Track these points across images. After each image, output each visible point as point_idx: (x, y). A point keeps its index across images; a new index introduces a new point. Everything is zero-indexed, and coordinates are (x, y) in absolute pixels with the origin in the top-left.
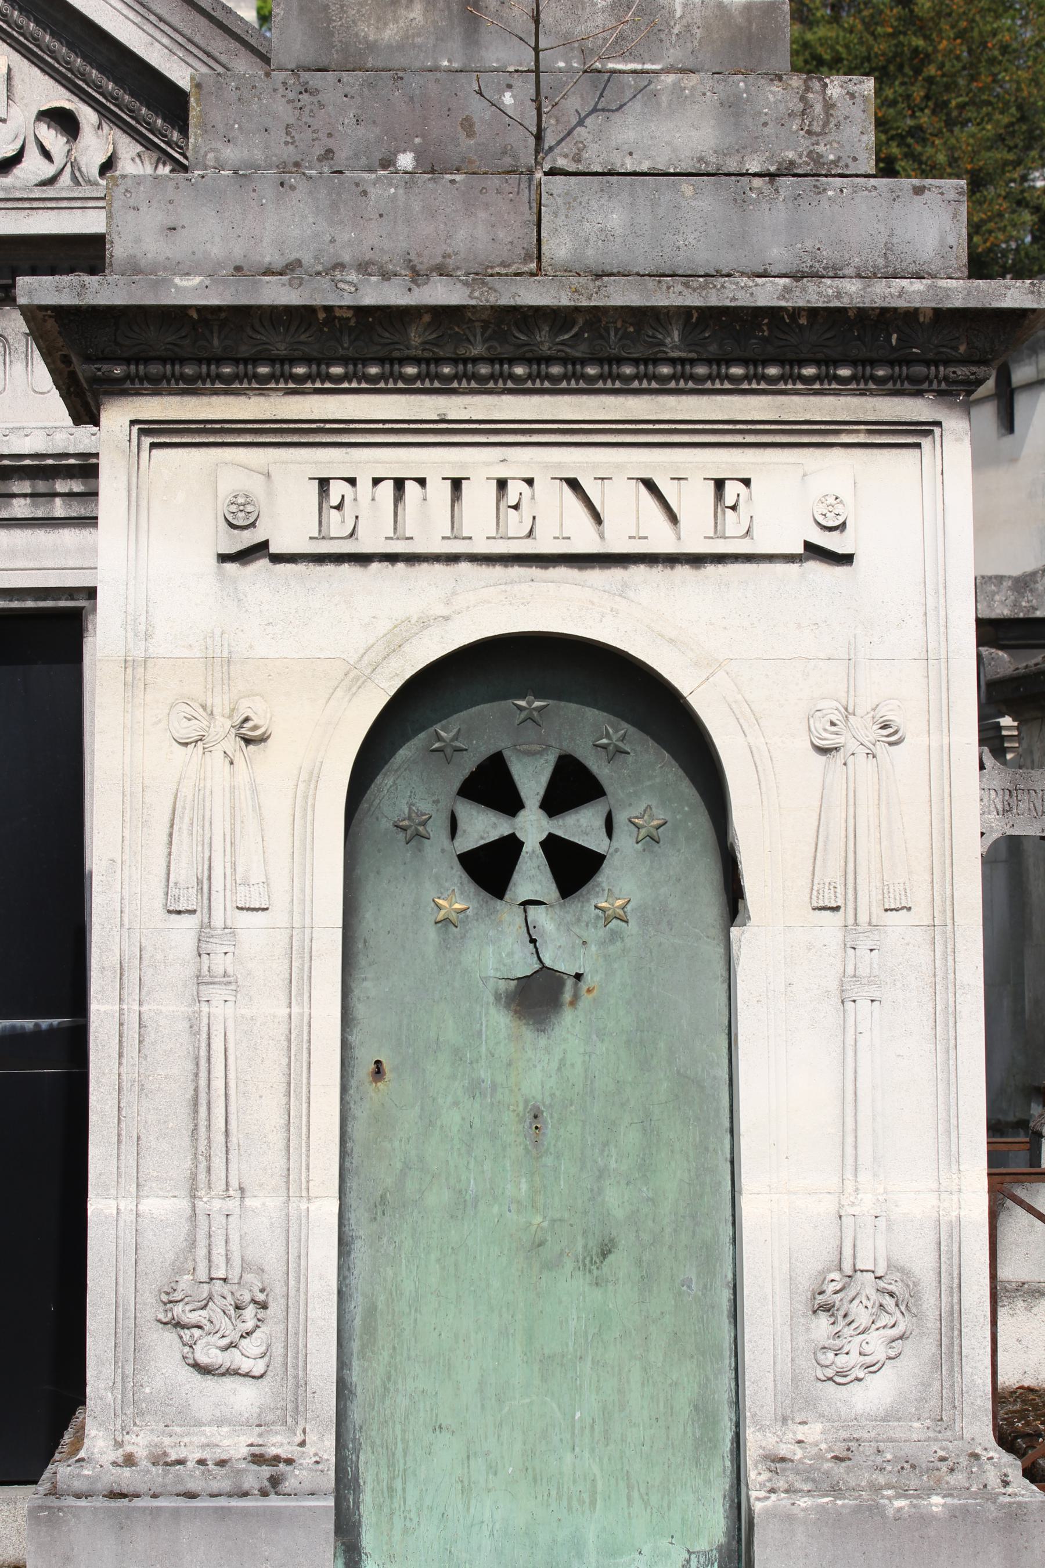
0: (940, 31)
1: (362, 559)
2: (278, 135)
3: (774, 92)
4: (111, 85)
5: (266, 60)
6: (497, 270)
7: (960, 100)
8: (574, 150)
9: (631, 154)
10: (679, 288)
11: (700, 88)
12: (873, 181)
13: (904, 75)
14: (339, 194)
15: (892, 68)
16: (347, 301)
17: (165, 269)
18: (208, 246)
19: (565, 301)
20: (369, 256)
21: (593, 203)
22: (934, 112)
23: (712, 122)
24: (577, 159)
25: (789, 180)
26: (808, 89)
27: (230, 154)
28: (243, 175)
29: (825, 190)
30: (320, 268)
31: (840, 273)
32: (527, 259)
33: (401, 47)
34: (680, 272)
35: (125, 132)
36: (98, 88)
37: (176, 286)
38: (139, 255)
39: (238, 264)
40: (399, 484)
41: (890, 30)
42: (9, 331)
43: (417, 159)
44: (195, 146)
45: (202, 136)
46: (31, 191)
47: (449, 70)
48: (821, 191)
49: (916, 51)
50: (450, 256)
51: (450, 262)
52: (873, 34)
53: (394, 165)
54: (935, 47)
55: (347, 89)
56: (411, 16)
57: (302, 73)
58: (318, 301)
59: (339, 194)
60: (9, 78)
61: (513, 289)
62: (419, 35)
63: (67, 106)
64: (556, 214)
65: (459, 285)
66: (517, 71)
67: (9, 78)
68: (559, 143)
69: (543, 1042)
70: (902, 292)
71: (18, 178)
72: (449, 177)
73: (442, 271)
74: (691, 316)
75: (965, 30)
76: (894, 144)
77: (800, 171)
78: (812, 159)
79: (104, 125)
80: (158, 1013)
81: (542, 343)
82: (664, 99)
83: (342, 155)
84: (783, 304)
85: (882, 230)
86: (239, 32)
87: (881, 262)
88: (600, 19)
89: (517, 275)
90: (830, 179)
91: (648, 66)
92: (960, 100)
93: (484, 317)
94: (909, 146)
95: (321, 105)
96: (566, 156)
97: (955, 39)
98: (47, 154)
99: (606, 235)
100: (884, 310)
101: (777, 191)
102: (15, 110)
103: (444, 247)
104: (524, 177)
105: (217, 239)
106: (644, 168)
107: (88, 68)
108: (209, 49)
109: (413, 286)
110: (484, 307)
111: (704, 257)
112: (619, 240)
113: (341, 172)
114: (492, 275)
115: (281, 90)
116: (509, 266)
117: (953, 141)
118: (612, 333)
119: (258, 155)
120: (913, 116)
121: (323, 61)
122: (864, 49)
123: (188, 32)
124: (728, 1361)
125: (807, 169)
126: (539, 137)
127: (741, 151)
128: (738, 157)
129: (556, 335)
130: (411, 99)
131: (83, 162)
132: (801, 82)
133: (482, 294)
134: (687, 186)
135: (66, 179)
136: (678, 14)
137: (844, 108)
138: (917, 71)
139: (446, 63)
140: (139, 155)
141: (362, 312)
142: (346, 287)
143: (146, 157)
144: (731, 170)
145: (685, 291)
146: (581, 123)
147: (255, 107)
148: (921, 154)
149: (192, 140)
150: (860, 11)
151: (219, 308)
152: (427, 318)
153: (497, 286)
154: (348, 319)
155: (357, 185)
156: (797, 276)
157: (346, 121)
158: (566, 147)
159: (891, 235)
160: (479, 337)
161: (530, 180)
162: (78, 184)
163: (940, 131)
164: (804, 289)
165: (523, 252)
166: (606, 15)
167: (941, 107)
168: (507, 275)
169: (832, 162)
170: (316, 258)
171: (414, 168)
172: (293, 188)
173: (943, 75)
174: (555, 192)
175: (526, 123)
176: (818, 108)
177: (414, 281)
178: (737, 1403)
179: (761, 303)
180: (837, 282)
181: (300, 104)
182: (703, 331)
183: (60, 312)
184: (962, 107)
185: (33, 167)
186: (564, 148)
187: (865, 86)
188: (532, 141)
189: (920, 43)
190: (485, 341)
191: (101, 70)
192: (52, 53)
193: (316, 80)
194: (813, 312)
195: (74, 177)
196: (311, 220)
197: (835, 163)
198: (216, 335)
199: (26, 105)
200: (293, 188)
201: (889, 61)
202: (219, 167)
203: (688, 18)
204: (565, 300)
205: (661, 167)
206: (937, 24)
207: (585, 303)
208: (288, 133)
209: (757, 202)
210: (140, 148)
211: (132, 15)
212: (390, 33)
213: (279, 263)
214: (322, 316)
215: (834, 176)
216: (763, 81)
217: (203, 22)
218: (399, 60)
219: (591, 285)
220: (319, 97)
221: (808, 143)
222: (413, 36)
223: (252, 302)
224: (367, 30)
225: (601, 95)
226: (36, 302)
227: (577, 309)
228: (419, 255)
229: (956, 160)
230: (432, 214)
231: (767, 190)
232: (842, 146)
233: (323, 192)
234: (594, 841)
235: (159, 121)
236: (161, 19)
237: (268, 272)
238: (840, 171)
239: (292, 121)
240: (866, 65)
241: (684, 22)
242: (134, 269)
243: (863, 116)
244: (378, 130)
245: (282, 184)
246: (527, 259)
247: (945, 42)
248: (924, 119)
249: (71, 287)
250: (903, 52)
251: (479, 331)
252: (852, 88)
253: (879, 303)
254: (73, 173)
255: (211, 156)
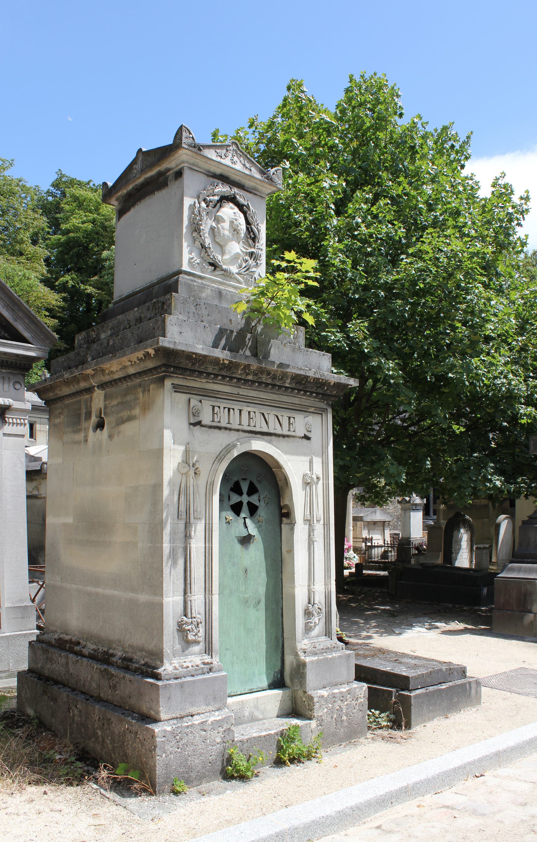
1: (220, 428)
40: (229, 409)
69: (247, 552)
80: (176, 546)
124: (281, 627)
178: (283, 636)
234: (256, 503)
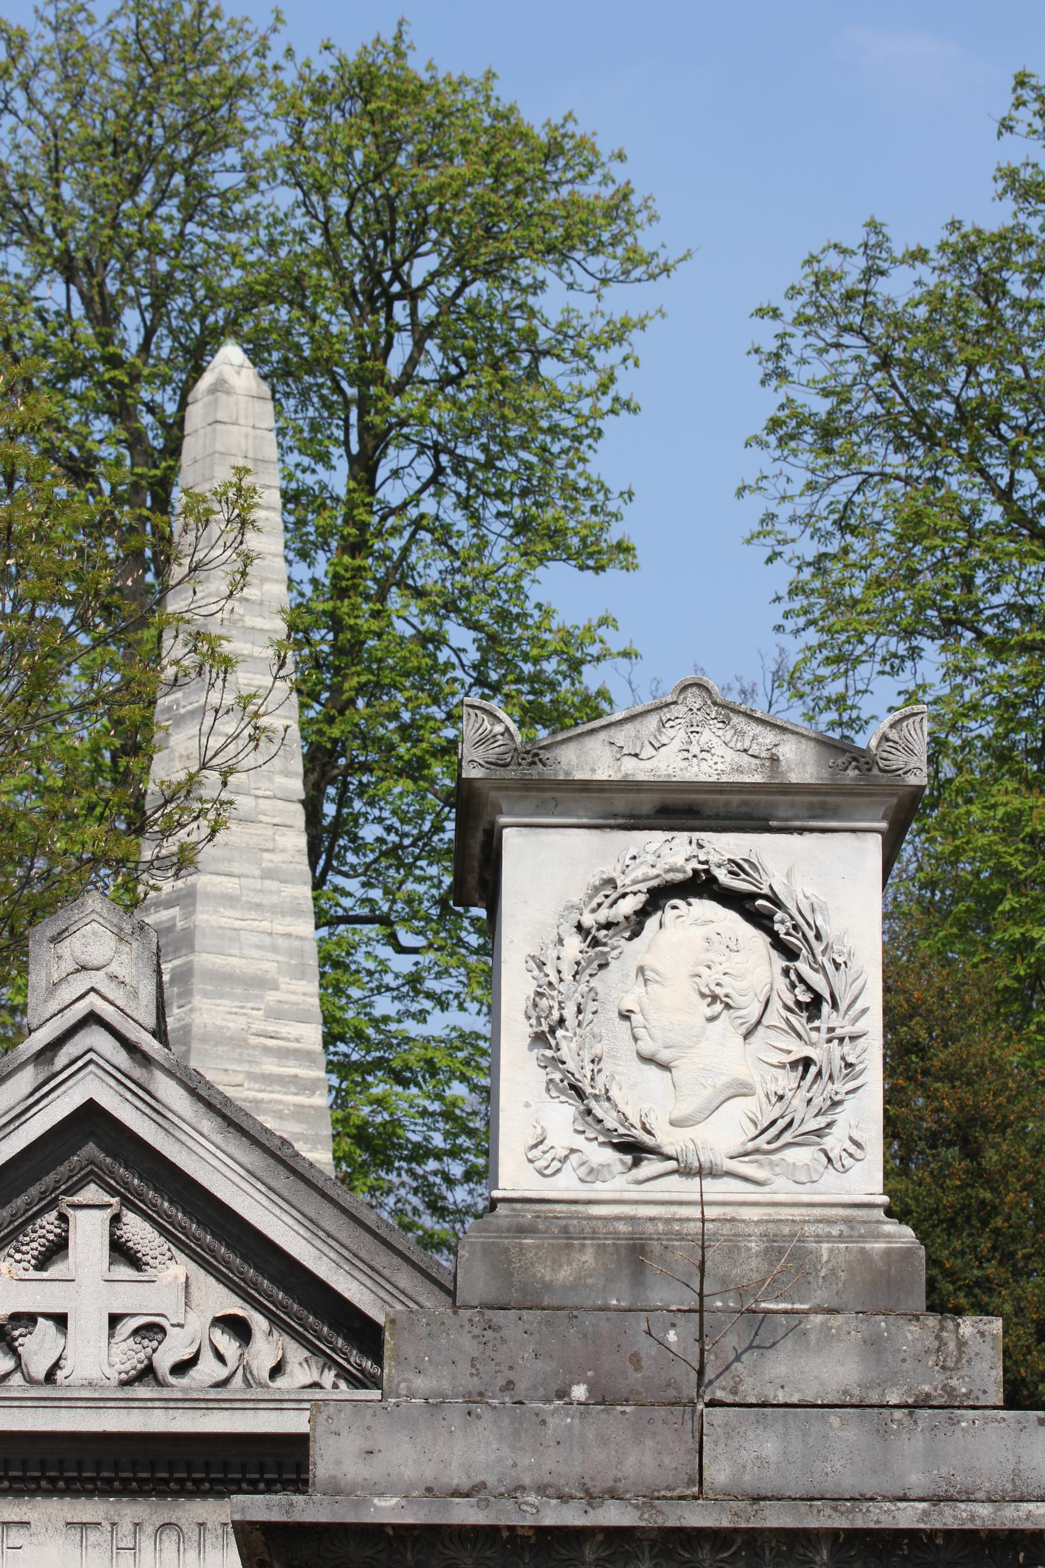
0: (1007, 1184)
2: (465, 1367)
3: (912, 1330)
4: (281, 1295)
5: (452, 1294)
6: (663, 1493)
7: (1026, 1251)
8: (732, 1383)
9: (782, 1387)
10: (828, 1511)
11: (846, 1328)
12: (1003, 1413)
13: (972, 1227)
14: (521, 1423)
15: (959, 1220)
16: (529, 1521)
17: (363, 1488)
18: (402, 1468)
19: (725, 1523)
20: (547, 1479)
21: (750, 1433)
22: (1000, 1263)
23: (856, 1358)
24: (734, 1392)
25: (927, 1413)
26: (942, 1328)
27: (420, 1383)
28: (435, 1404)
29: (959, 1422)
30: (502, 1490)
31: (972, 1497)
32: (690, 1483)
33: (574, 1287)
34: (828, 1496)
35: (293, 1338)
36: (269, 1297)
37: (375, 1506)
38: (340, 1476)
39: (429, 1485)
41: (958, 1183)
42: (183, 1520)
43: (589, 1390)
44: (389, 1376)
45: (395, 1367)
46: (208, 1393)
47: (618, 1310)
48: (955, 1422)
49: (983, 1203)
50: (620, 1480)
51: (621, 1485)
52: (941, 1186)
53: (569, 1396)
54: (1002, 1200)
55: (527, 1326)
56: (584, 1259)
57: (486, 1311)
58: (503, 1521)
59: (521, 1423)
60: (187, 1286)
61: (679, 1512)
62: (590, 1276)
63: (240, 1313)
64: (716, 1443)
65: (630, 1508)
66: (679, 1310)
67: (187, 1286)
68: (718, 1377)
70: (1029, 1515)
71: (194, 1379)
72: (619, 1408)
73: (614, 1494)
74: (839, 1536)
75: (1031, 1183)
76: (962, 1294)
77: (935, 1403)
78: (946, 1392)
79: (275, 1332)
81: (704, 1560)
82: (813, 1337)
83: (522, 1386)
84: (922, 1526)
85: (1010, 1457)
86: (401, 1248)
87: (1009, 1487)
88: (754, 1263)
89: (682, 1498)
90: (964, 1412)
91: (797, 1306)
92: (1026, 1251)
93: (651, 1536)
94: (975, 1296)
95: (503, 1340)
96: (724, 1389)
97: (1022, 1191)
98: (221, 1358)
99: (762, 1462)
100: (1012, 1532)
101: (915, 1422)
102: (192, 1316)
103: (615, 1472)
104: (688, 1409)
105: (410, 1462)
106: (795, 1400)
107: (260, 1278)
108: (373, 1263)
109: (589, 1509)
110: (653, 1528)
111: (849, 1483)
112: (773, 1467)
113: (521, 1403)
114: (658, 1498)
115: (467, 1327)
116: (673, 1489)
117: (1019, 1291)
118: (767, 1552)
119: (446, 1385)
120: (980, 1267)
121: (504, 1299)
122: (932, 1201)
123: (354, 1248)
125: (942, 1401)
126: (701, 1373)
127: (882, 1385)
128: (879, 1390)
129: (717, 1553)
130: (585, 1336)
131: (254, 1365)
132: (936, 1322)
133: (651, 1516)
134: (834, 1418)
135: (238, 1381)
136: (825, 1258)
137: (975, 1345)
138: (985, 1223)
139: (614, 1302)
140: (306, 1360)
141: (542, 1531)
142: (528, 1508)
143: (313, 1361)
144: (874, 1402)
145: (834, 1515)
146: (738, 1358)
147: (443, 1341)
148: (988, 1304)
149: (386, 1371)
150: (928, 1164)
151: (413, 1527)
152: (600, 1537)
153: (665, 1510)
154: (529, 1537)
155: (537, 1415)
156: (935, 1500)
157: (526, 1355)
158: (725, 1381)
159: (1018, 1462)
160: (647, 1554)
161: (693, 1412)
162: (249, 1386)
163: (1007, 1281)
164: (941, 1513)
165: (686, 1477)
166: (759, 1259)
167: (1007, 1258)
168: (671, 1498)
169: (964, 1395)
170: (500, 1480)
171: (587, 1398)
172: (479, 1417)
173: (1010, 1227)
174: (716, 1423)
175: (688, 1359)
176: (952, 1345)
177: (589, 1504)
179: (903, 1525)
180: (971, 1506)
181: (484, 1340)
182: (850, 1550)
183: (267, 1527)
184: (1027, 1257)
185: (208, 1369)
186: (722, 1381)
187: (994, 1326)
188: (694, 1376)
189: (988, 1195)
190: (652, 1558)
191: (272, 1280)
192: (227, 1264)
193: (499, 1317)
194: (948, 1534)
195: (246, 1380)
196: (495, 1446)
197: (967, 1395)
198: (409, 1550)
199: (202, 1311)
200: (479, 1417)
201: (957, 1213)
202: (411, 1395)
203: (833, 1262)
204: (726, 1522)
205: (810, 1399)
206: (1004, 1177)
207: (743, 1525)
208: (473, 1366)
209: (897, 1433)
210: (307, 1354)
211: (302, 1231)
212: (564, 1274)
213: (466, 1484)
214: (505, 1534)
215: (967, 1407)
216: (902, 1322)
217: (368, 1238)
218: (573, 1300)
219: (749, 1509)
220: (502, 1333)
221: (942, 1377)
222: (585, 1277)
223: (444, 1521)
224: (544, 1272)
225: (756, 1334)
226: (248, 1518)
227: (736, 1530)
228: (592, 1479)
229: (1022, 1310)
230: (603, 1441)
231: (906, 1421)
232: (973, 1380)
233: (506, 1421)
235: (325, 1329)
236: (329, 1235)
237: (457, 1493)
238: (971, 1403)
239: (477, 1354)
240: (935, 1217)
241: (830, 1266)
242: (336, 1490)
243: (992, 1353)
244: (554, 1364)
245: (469, 1414)
246: (690, 1483)
247: (1011, 1195)
248: (991, 1269)
249: (280, 1505)
250: (970, 1205)
251: (647, 1549)
252: (982, 1327)
253: (1009, 1525)
254: (244, 1375)
255: (403, 1385)
